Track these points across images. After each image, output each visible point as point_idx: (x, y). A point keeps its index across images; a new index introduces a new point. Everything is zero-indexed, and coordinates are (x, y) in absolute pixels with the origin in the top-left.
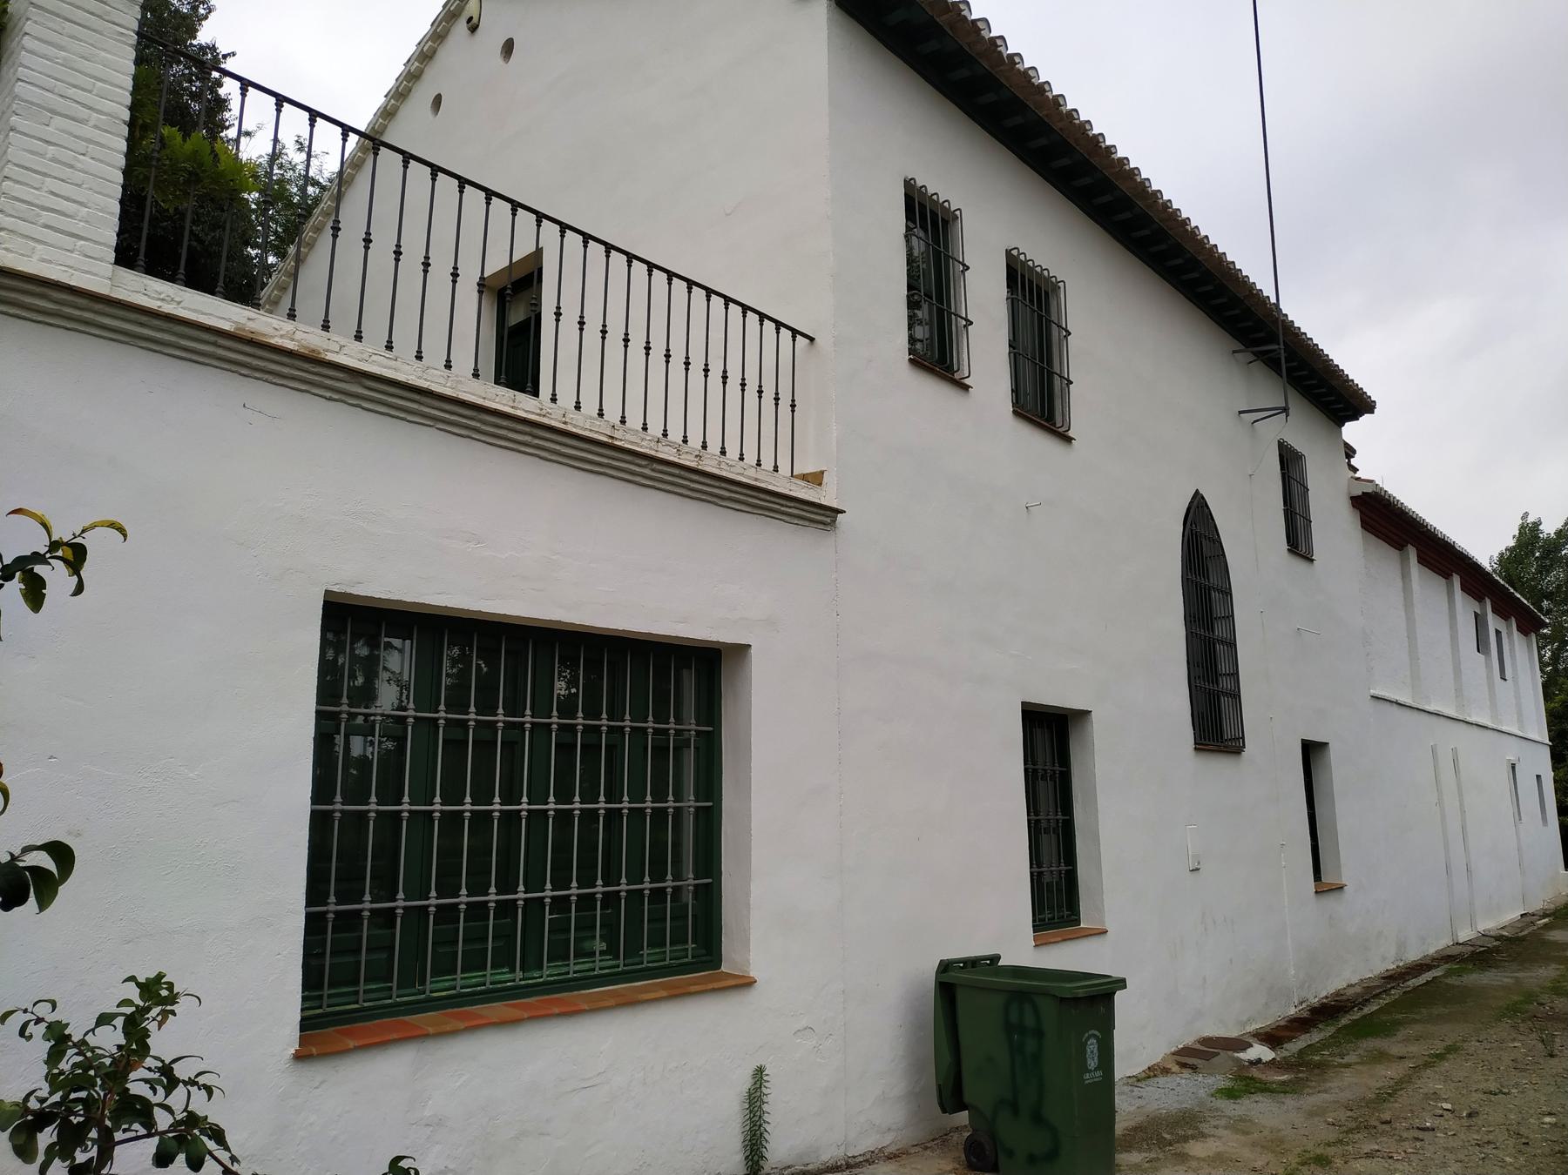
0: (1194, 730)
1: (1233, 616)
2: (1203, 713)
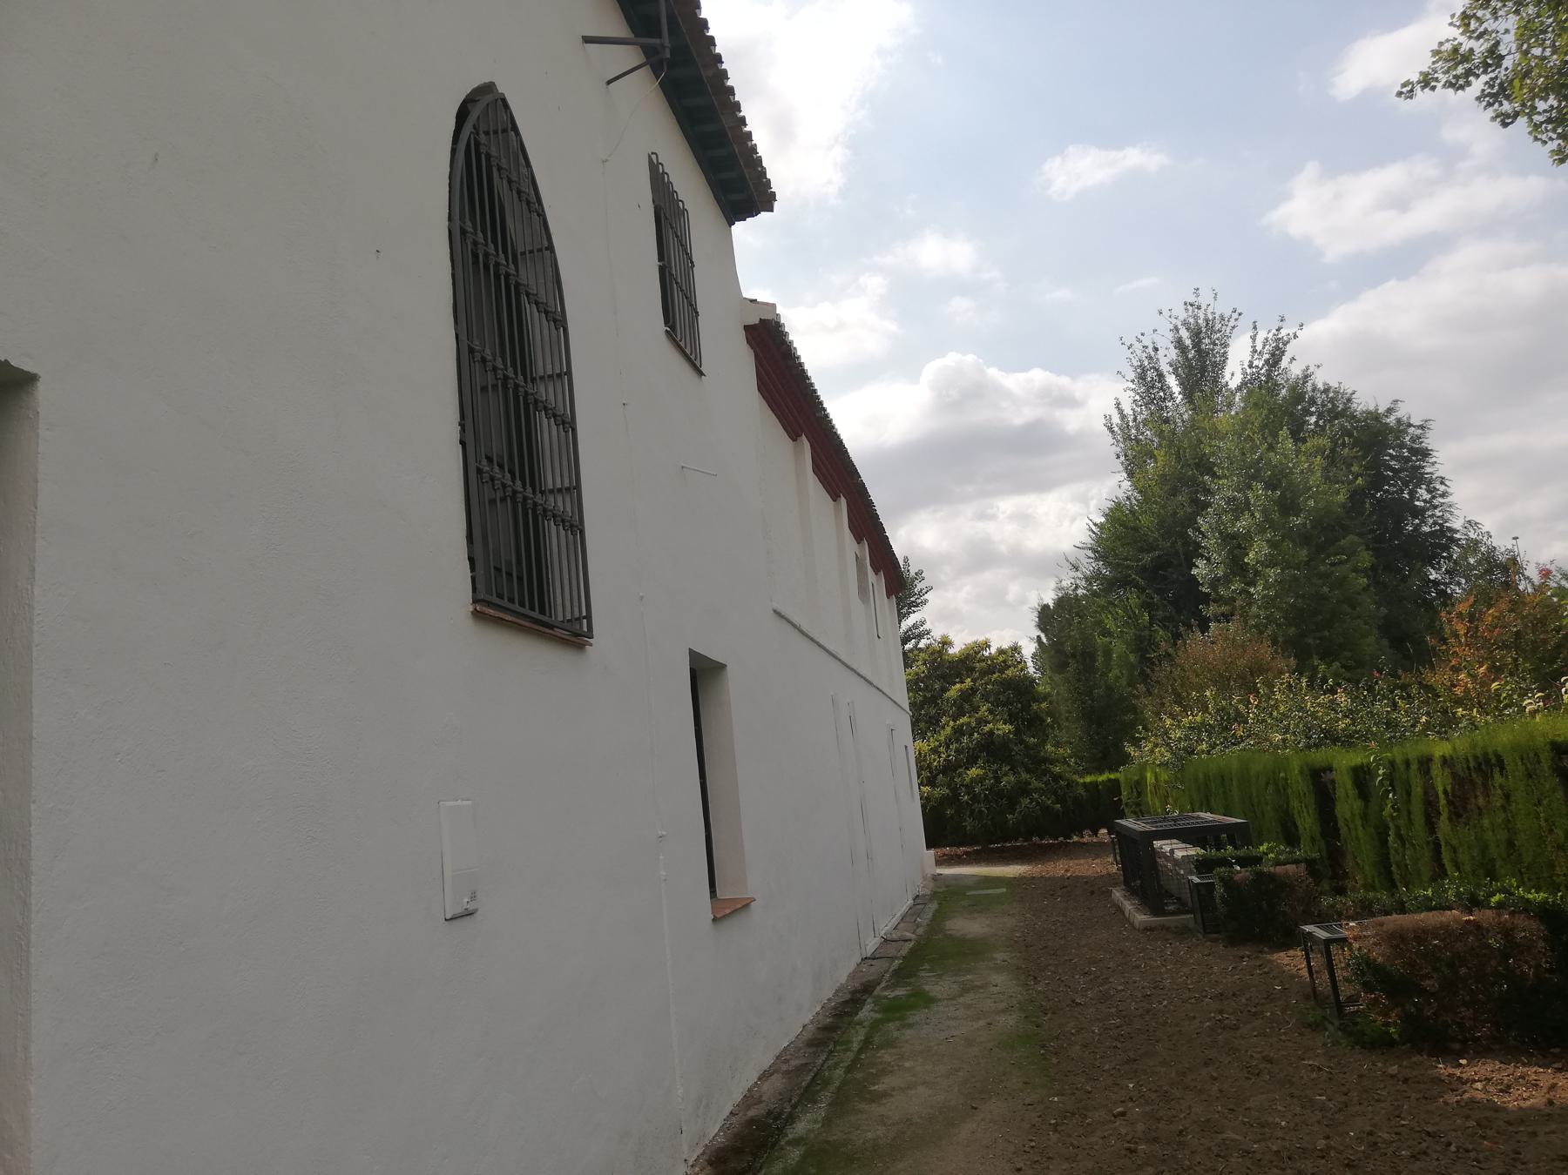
0: (473, 569)
1: (569, 373)
2: (509, 563)
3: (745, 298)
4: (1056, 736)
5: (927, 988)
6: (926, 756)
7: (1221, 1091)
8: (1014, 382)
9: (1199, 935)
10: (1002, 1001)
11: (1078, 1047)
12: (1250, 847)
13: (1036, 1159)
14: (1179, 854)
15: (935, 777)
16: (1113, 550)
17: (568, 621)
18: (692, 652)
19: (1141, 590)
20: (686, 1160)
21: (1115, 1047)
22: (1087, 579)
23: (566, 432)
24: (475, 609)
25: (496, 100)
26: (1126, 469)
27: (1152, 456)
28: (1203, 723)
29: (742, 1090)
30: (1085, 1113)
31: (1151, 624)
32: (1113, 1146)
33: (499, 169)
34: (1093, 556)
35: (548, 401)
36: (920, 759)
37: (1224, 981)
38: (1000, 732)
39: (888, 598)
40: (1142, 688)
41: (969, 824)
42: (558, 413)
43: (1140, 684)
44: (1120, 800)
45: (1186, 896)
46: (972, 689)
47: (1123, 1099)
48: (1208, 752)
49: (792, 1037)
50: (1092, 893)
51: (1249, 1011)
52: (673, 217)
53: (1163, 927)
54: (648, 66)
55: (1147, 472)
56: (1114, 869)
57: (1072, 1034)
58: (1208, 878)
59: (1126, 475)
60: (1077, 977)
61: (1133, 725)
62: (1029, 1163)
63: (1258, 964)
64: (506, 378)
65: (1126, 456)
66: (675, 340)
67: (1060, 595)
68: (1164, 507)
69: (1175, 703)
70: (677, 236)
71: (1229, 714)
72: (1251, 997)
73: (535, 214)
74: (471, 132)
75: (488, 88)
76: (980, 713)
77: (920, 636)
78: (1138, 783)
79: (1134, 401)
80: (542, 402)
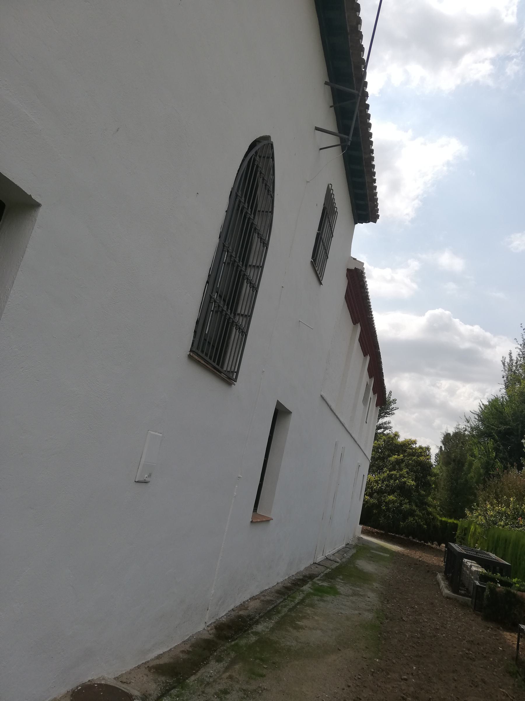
1: (262, 267)
3: (351, 257)
4: (435, 494)
5: (338, 587)
6: (371, 483)
7: (456, 687)
8: (464, 329)
9: (471, 609)
10: (369, 606)
11: (396, 640)
12: (509, 578)
13: (358, 684)
14: (474, 569)
15: (373, 493)
16: (488, 419)
17: (228, 371)
18: (278, 403)
19: (495, 441)
20: (206, 623)
21: (413, 647)
22: (472, 428)
23: (253, 291)
25: (269, 144)
26: (505, 384)
27: (519, 382)
28: (505, 512)
30: (388, 672)
31: (495, 458)
32: (396, 693)
34: (477, 418)
36: (369, 483)
37: (476, 635)
38: (409, 484)
39: (376, 406)
40: (481, 486)
41: (382, 520)
42: (252, 282)
43: (481, 484)
44: (455, 534)
45: (471, 589)
46: (402, 460)
47: (408, 673)
48: (503, 526)
49: (271, 586)
50: (428, 571)
51: (483, 654)
53: (455, 599)
55: (514, 389)
56: (442, 564)
57: (396, 633)
58: (483, 584)
59: (504, 387)
60: (408, 607)
61: (473, 502)
62: (355, 685)
63: (494, 634)
64: (235, 261)
65: (507, 378)
67: (457, 431)
68: (518, 407)
69: (495, 498)
70: (329, 222)
71: (519, 512)
72: (486, 648)
74: (253, 155)
75: (267, 138)
76: (402, 472)
77: (386, 428)
78: (466, 529)
79: (519, 354)
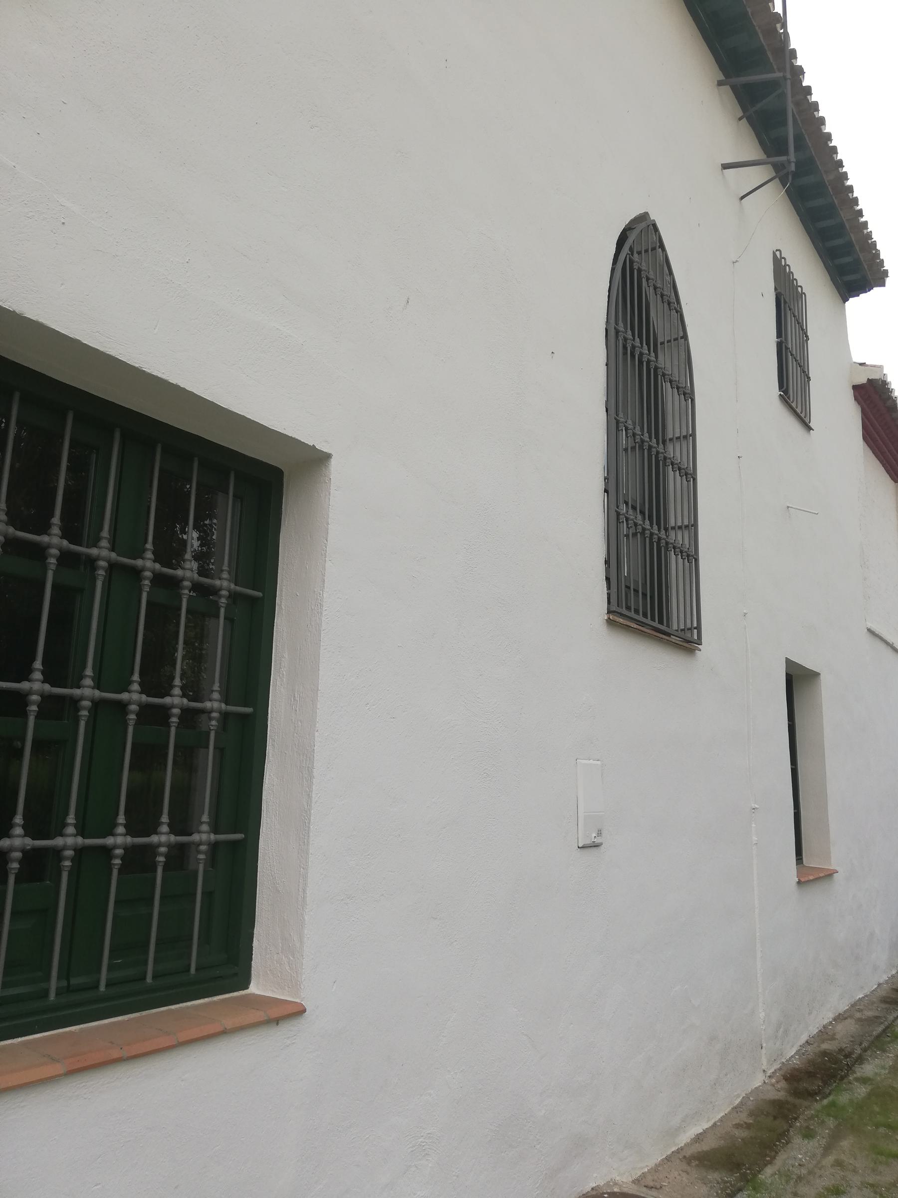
0: (609, 588)
1: (693, 435)
2: (636, 582)
3: (855, 363)
17: (682, 630)
18: (789, 662)
20: (764, 1071)
24: (609, 618)
29: (818, 1026)
33: (648, 279)
35: (675, 458)
49: (867, 991)
52: (792, 301)
54: (777, 179)
66: (787, 402)
70: (794, 316)
73: (675, 311)
75: (643, 218)
80: (670, 458)
